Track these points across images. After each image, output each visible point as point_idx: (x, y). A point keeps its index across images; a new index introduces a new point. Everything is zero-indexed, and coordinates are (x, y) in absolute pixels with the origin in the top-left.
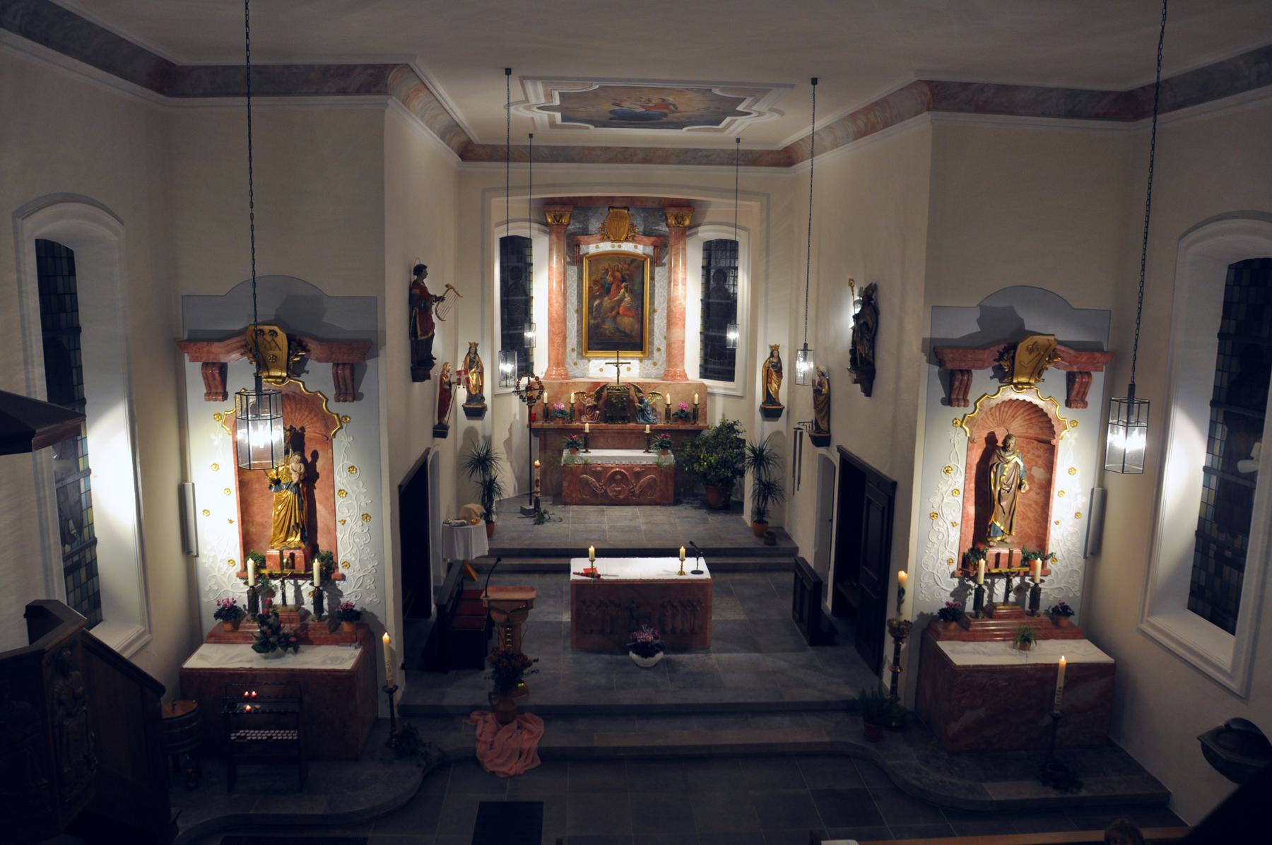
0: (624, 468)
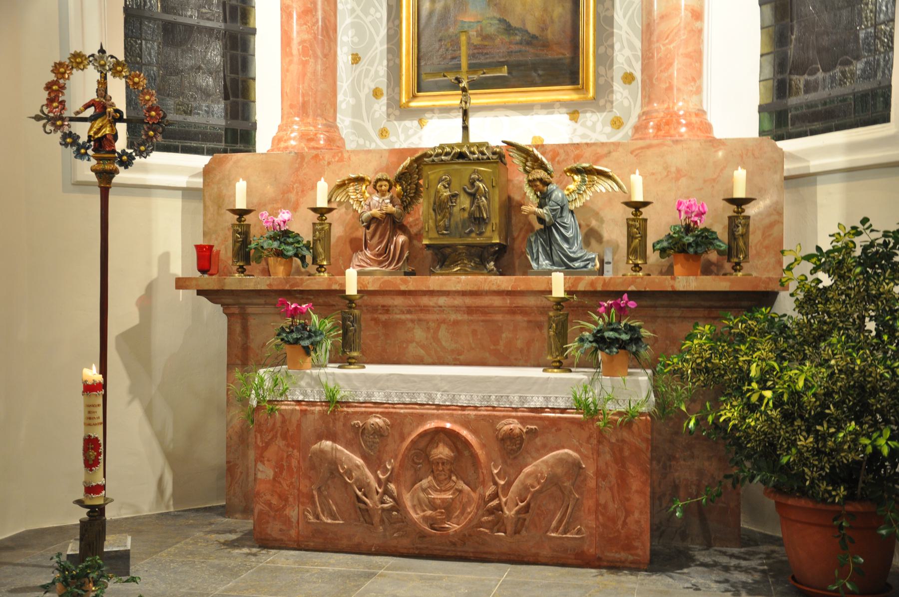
0: (466, 423)
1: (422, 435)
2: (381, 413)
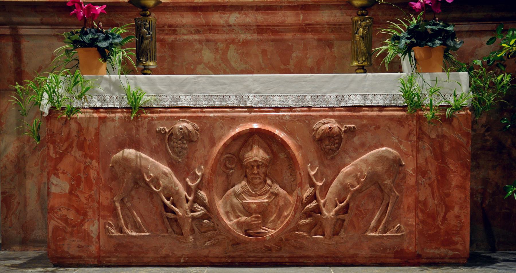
1: (235, 138)
2: (189, 118)
